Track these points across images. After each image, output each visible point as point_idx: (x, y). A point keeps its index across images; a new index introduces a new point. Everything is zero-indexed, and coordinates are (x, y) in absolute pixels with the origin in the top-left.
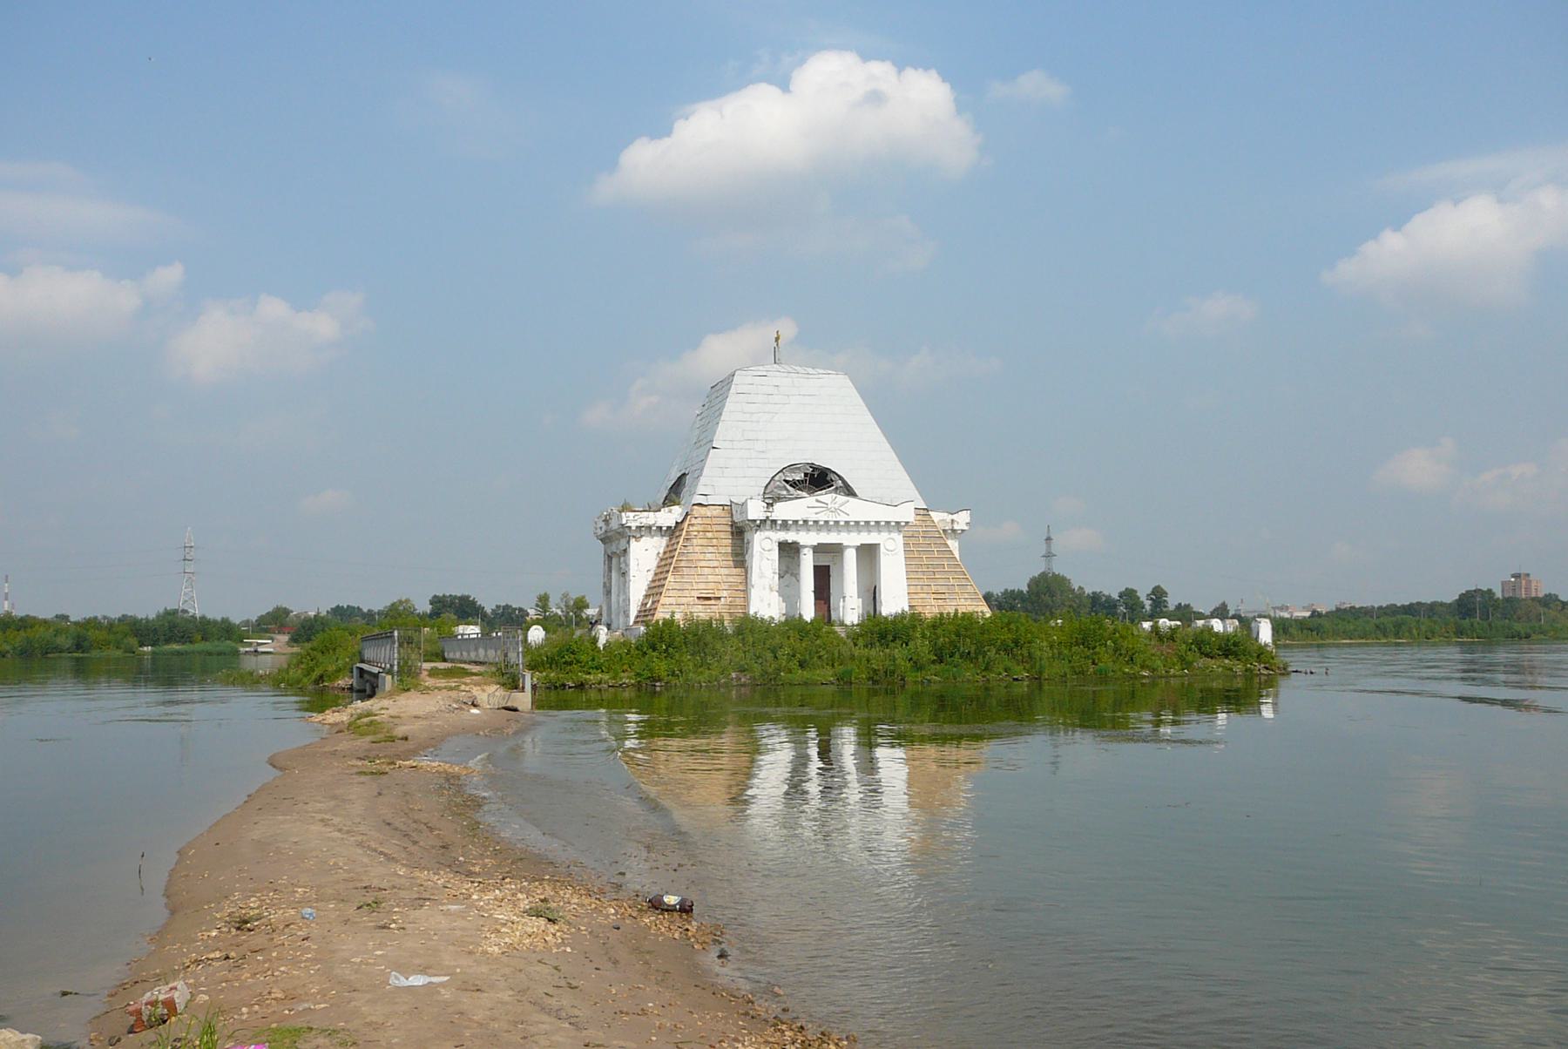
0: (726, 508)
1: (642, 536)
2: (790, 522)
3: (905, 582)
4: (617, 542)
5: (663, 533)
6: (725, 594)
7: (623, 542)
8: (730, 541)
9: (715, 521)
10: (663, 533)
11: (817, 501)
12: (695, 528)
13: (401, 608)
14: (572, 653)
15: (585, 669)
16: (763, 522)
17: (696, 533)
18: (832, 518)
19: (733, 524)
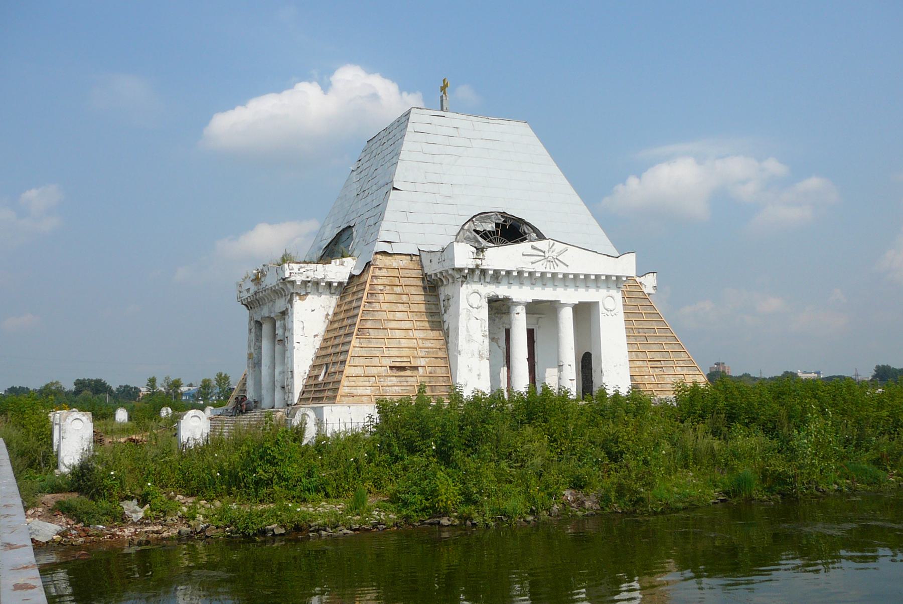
0: (414, 258)
1: (307, 294)
2: (503, 273)
3: (625, 349)
4: (271, 303)
5: (333, 291)
6: (422, 362)
7: (280, 305)
8: (423, 298)
9: (403, 273)
10: (333, 291)
11: (533, 248)
12: (380, 281)
13: (53, 388)
14: (269, 462)
15: (296, 493)
16: (472, 271)
17: (381, 287)
18: (549, 269)
19: (425, 277)
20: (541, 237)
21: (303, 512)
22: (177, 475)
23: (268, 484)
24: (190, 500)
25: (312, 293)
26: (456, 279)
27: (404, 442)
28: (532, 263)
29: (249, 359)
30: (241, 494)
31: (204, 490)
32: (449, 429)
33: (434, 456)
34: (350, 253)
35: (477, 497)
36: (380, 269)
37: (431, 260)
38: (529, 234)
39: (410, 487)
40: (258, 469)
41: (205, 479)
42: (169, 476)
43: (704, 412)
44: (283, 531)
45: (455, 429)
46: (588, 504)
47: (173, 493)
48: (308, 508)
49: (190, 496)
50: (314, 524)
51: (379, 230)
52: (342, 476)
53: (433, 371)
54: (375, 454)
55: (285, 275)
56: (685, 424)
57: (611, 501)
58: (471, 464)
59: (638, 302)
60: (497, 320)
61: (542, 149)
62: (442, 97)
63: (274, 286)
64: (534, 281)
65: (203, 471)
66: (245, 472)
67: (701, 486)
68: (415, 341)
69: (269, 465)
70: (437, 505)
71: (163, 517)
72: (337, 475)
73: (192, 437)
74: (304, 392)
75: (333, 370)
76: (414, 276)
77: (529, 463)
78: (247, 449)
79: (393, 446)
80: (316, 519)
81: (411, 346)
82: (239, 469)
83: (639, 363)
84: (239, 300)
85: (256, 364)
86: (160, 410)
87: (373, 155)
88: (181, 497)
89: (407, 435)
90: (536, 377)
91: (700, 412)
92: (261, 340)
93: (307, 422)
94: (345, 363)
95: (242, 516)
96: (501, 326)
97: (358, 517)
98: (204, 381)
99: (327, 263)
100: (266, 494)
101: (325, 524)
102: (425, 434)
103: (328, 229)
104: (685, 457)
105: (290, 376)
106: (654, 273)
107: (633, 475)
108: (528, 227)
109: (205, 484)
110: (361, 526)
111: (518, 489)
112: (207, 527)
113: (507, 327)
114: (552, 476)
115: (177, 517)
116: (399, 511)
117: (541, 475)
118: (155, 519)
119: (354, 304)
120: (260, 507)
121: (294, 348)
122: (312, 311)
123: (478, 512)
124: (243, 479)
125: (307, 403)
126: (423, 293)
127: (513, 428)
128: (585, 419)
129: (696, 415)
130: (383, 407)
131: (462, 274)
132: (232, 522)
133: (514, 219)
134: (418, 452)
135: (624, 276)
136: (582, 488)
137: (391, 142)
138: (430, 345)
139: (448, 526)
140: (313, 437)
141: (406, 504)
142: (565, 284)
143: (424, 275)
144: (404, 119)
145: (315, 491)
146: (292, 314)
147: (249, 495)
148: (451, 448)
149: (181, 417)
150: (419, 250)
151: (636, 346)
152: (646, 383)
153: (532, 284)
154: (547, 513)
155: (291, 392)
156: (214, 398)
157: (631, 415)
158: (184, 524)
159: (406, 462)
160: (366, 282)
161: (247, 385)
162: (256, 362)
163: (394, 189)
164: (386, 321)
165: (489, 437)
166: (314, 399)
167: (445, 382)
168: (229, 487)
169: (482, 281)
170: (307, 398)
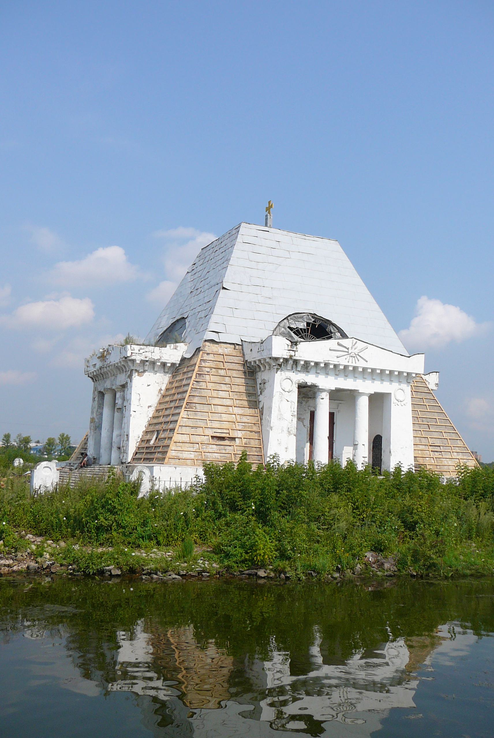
0: (237, 347)
1: (144, 371)
2: (313, 364)
3: (411, 434)
4: (113, 378)
6: (239, 434)
7: (121, 379)
8: (243, 381)
9: (227, 359)
11: (339, 344)
12: (207, 364)
15: (131, 540)
16: (286, 360)
17: (208, 370)
18: (352, 363)
19: (245, 363)
20: (344, 336)
21: (138, 557)
22: (29, 517)
23: (107, 530)
24: (39, 539)
25: (148, 371)
26: (272, 366)
27: (228, 501)
28: (337, 357)
29: (91, 422)
30: (84, 538)
31: (51, 531)
32: (268, 492)
33: (253, 515)
34: (182, 340)
35: (290, 553)
36: (208, 354)
37: (251, 350)
38: (335, 333)
39: (232, 541)
40: (100, 517)
41: (52, 522)
42: (22, 518)
43: (485, 492)
44: (119, 572)
45: (273, 493)
46: (387, 566)
47: (24, 532)
48: (141, 553)
49: (38, 536)
50: (146, 568)
51: (208, 322)
52: (172, 527)
53: (247, 443)
54: (202, 510)
55: (127, 354)
56: (468, 501)
57: (407, 565)
58: (285, 523)
59: (423, 396)
60: (304, 403)
61: (348, 264)
62: (267, 216)
63: (117, 363)
64: (337, 373)
65: (51, 515)
66: (88, 518)
67: (484, 556)
68: (234, 416)
69: (109, 513)
70: (255, 558)
71: (14, 553)
72: (168, 526)
73: (43, 484)
74: (136, 453)
75: (163, 436)
76: (236, 362)
77: (336, 526)
78: (91, 498)
79: (218, 504)
80: (148, 564)
81: (230, 420)
82: (83, 516)
83: (422, 447)
84: (86, 373)
85: (97, 426)
86: (14, 460)
87: (207, 260)
88: (31, 536)
89: (230, 495)
90: (334, 453)
91: (482, 491)
92: (103, 408)
93: (143, 478)
94: (174, 431)
95: (84, 557)
96: (306, 409)
97: (186, 564)
98: (49, 440)
99: (163, 347)
100: (105, 538)
101: (157, 569)
102: (246, 495)
103: (165, 319)
104: (470, 530)
105: (126, 439)
106: (436, 372)
107: (428, 543)
108: (334, 327)
109: (52, 526)
110: (188, 572)
111: (326, 549)
112: (53, 564)
113: (312, 409)
114: (355, 539)
115: (27, 554)
116: (221, 562)
117: (345, 538)
118: (7, 554)
119: (184, 382)
120: (100, 550)
121: (131, 415)
122: (148, 386)
123: (291, 567)
124: (86, 524)
125: (139, 462)
126: (244, 377)
127: (321, 495)
128: (384, 491)
129: (478, 494)
130: (209, 470)
131: (278, 362)
132: (75, 561)
133: (322, 320)
134: (239, 510)
135: (414, 373)
136: (381, 551)
137: (222, 250)
138: (246, 421)
139: (264, 578)
140: (147, 492)
141: (228, 556)
142: (354, 375)
143: (245, 361)
144: (234, 232)
145: (148, 539)
146: (131, 387)
147: (90, 538)
148: (268, 509)
149: (32, 469)
150: (242, 341)
151: (420, 432)
152: (427, 464)
153: (336, 375)
154: (351, 572)
155: (126, 452)
156: (56, 454)
157: (424, 491)
158: (33, 560)
159: (228, 519)
160: (196, 364)
161: (88, 444)
162: (97, 425)
163: (224, 288)
164: (210, 398)
165: (303, 502)
166: (145, 459)
167: (257, 452)
168: (74, 530)
169: (294, 370)
170: (139, 458)
